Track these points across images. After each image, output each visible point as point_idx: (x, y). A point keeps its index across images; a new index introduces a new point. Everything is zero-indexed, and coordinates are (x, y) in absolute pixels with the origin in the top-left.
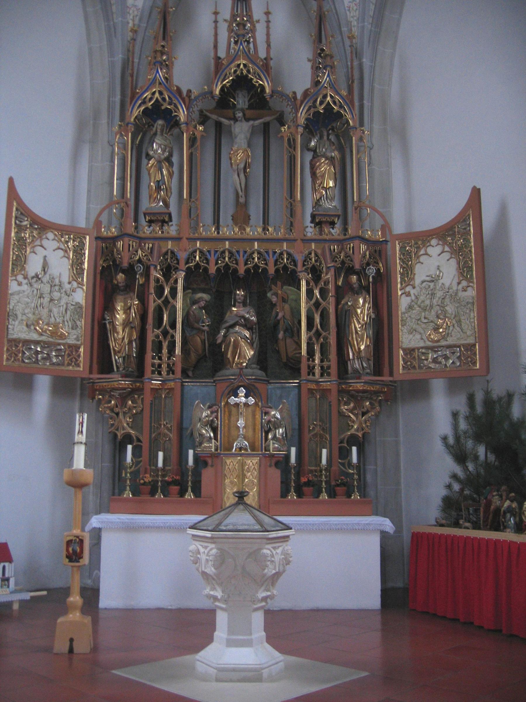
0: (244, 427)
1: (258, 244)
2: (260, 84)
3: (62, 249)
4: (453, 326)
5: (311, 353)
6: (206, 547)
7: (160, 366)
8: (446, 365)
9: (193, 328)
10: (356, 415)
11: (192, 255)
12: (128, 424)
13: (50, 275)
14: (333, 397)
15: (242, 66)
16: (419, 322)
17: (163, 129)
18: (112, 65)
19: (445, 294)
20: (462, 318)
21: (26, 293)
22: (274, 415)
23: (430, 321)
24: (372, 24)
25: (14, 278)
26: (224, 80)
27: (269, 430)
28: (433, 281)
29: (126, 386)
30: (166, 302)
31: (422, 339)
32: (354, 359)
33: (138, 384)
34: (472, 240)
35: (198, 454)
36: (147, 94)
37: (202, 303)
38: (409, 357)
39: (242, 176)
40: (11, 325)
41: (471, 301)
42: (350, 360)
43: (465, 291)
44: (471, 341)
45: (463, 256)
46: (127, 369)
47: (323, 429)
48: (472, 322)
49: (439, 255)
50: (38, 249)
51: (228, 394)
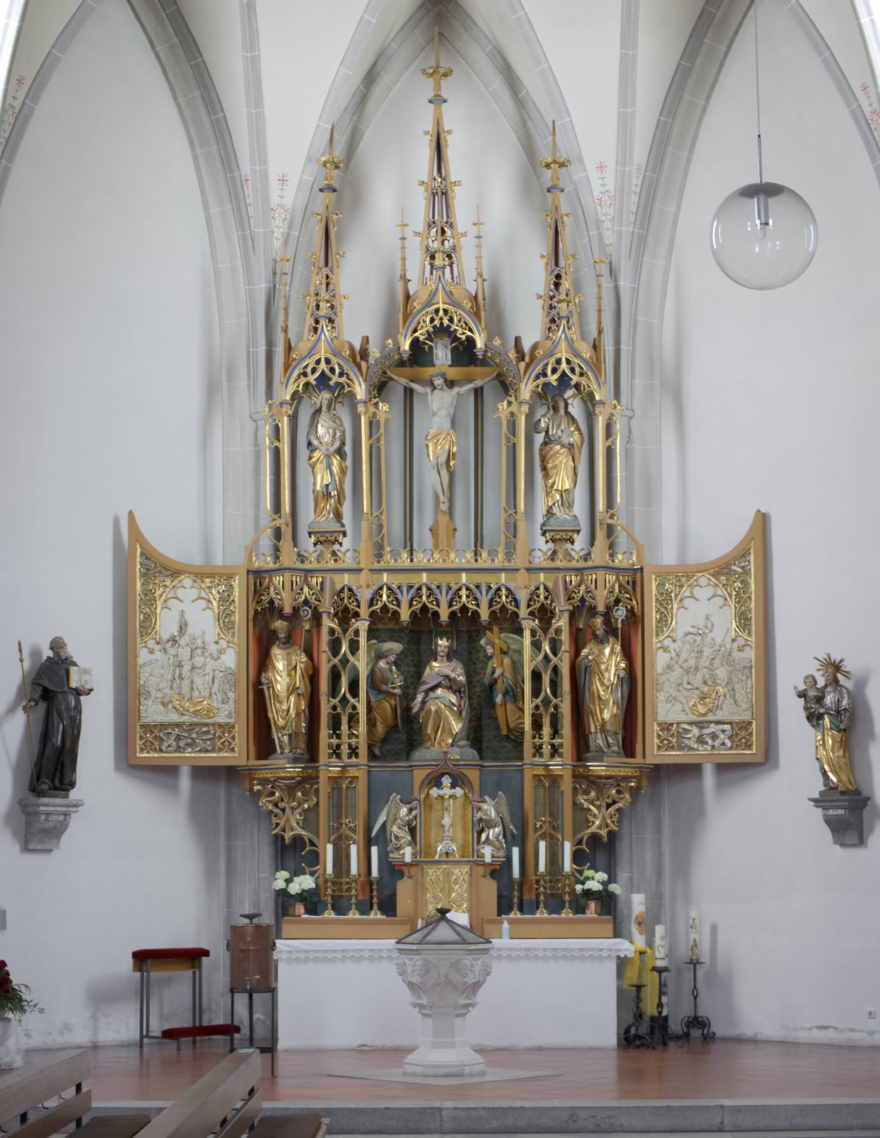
0: (452, 825)
1: (466, 576)
2: (468, 337)
3: (203, 598)
7: (338, 746)
9: (380, 691)
10: (599, 807)
11: (378, 593)
12: (298, 823)
13: (189, 635)
14: (567, 785)
15: (441, 313)
16: (680, 688)
17: (331, 405)
18: (251, 294)
19: (714, 653)
20: (737, 686)
21: (159, 663)
23: (694, 687)
24: (635, 223)
25: (143, 645)
26: (415, 331)
29: (295, 775)
30: (345, 661)
31: (684, 711)
33: (310, 771)
35: (392, 862)
37: (391, 657)
38: (666, 733)
39: (445, 474)
40: (144, 705)
41: (748, 665)
42: (591, 733)
44: (746, 717)
45: (741, 604)
46: (294, 751)
47: (554, 828)
48: (749, 693)
51: (429, 784)
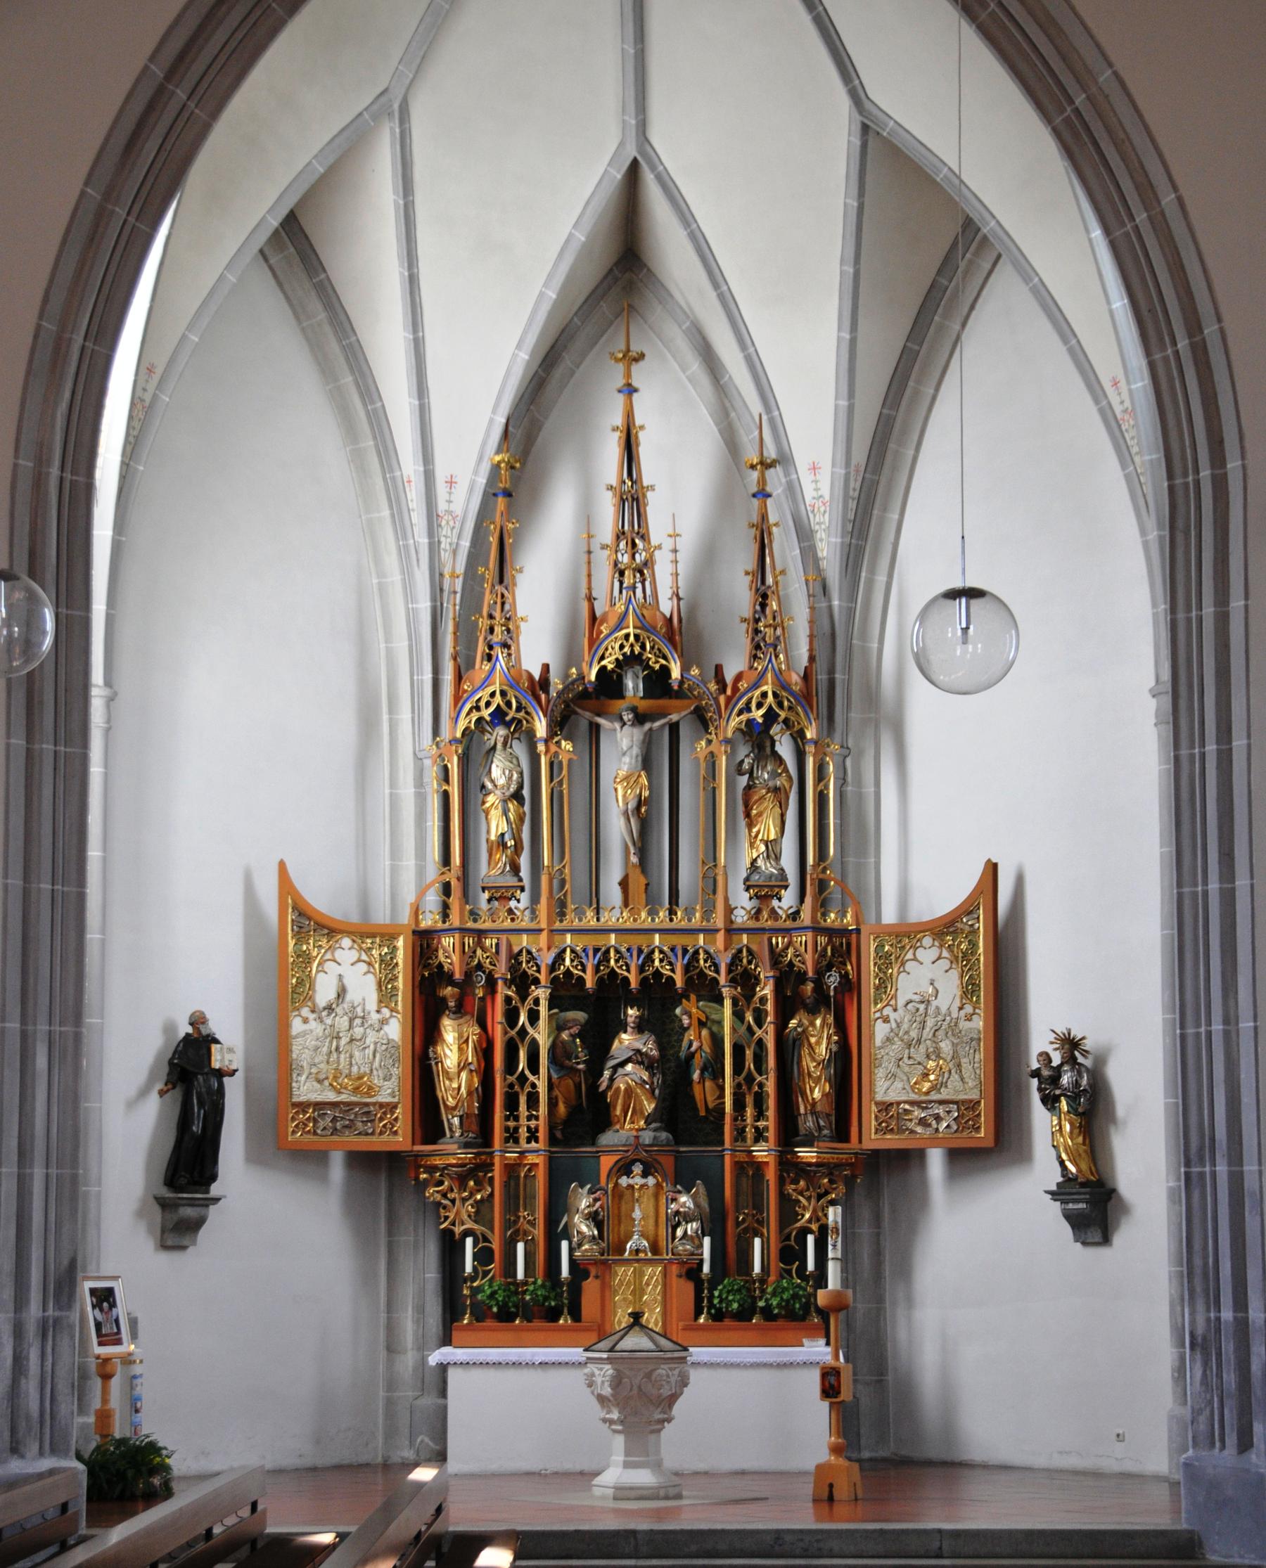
3: (364, 961)
4: (950, 1072)
5: (739, 1105)
7: (516, 1129)
8: (937, 1130)
10: (809, 1199)
11: (560, 957)
12: (469, 1216)
15: (632, 639)
22: (685, 1203)
26: (602, 658)
27: (679, 1224)
28: (923, 1002)
32: (806, 1114)
34: (981, 944)
36: (484, 694)
41: (975, 1036)
43: (969, 1020)
44: (974, 1095)
49: (933, 963)
50: (329, 966)
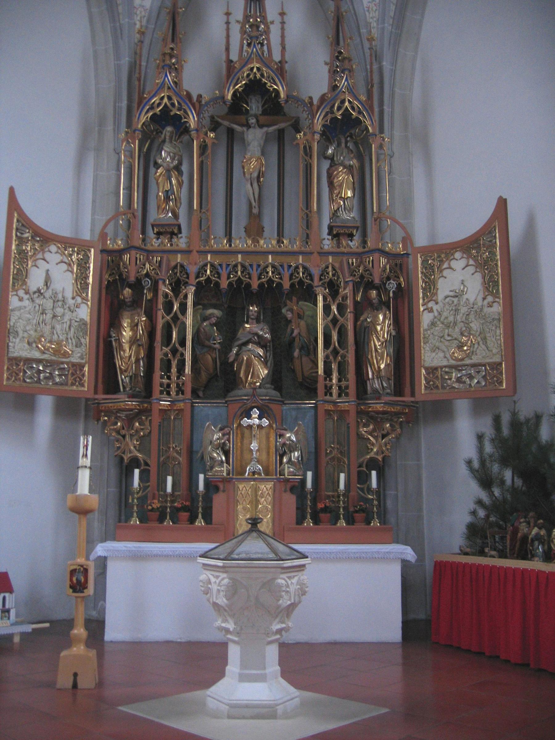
0: (258, 450)
1: (272, 257)
2: (274, 89)
3: (65, 263)
4: (478, 343)
5: (328, 372)
6: (217, 577)
7: (168, 386)
8: (470, 385)
9: (203, 346)
10: (376, 438)
11: (202, 269)
12: (135, 447)
13: (52, 290)
14: (352, 418)
15: (255, 70)
16: (442, 340)
17: (172, 136)
18: (118, 68)
19: (469, 310)
20: (488, 335)
21: (27, 309)
22: (290, 437)
23: (454, 338)
24: (392, 25)
25: (15, 293)
26: (236, 84)
27: (284, 453)
28: (457, 296)
29: (133, 407)
30: (175, 318)
31: (445, 357)
32: (373, 378)
33: (146, 405)
34: (498, 253)
35: (209, 478)
36: (156, 99)
37: (213, 319)
38: (431, 376)
39: (255, 185)
40: (12, 342)
41: (497, 317)
42: (369, 379)
43: (491, 306)
44: (497, 359)
45: (489, 270)
46: (134, 389)
47: (341, 453)
48: (499, 339)
49: (463, 269)
50: (41, 263)
51: (241, 415)
